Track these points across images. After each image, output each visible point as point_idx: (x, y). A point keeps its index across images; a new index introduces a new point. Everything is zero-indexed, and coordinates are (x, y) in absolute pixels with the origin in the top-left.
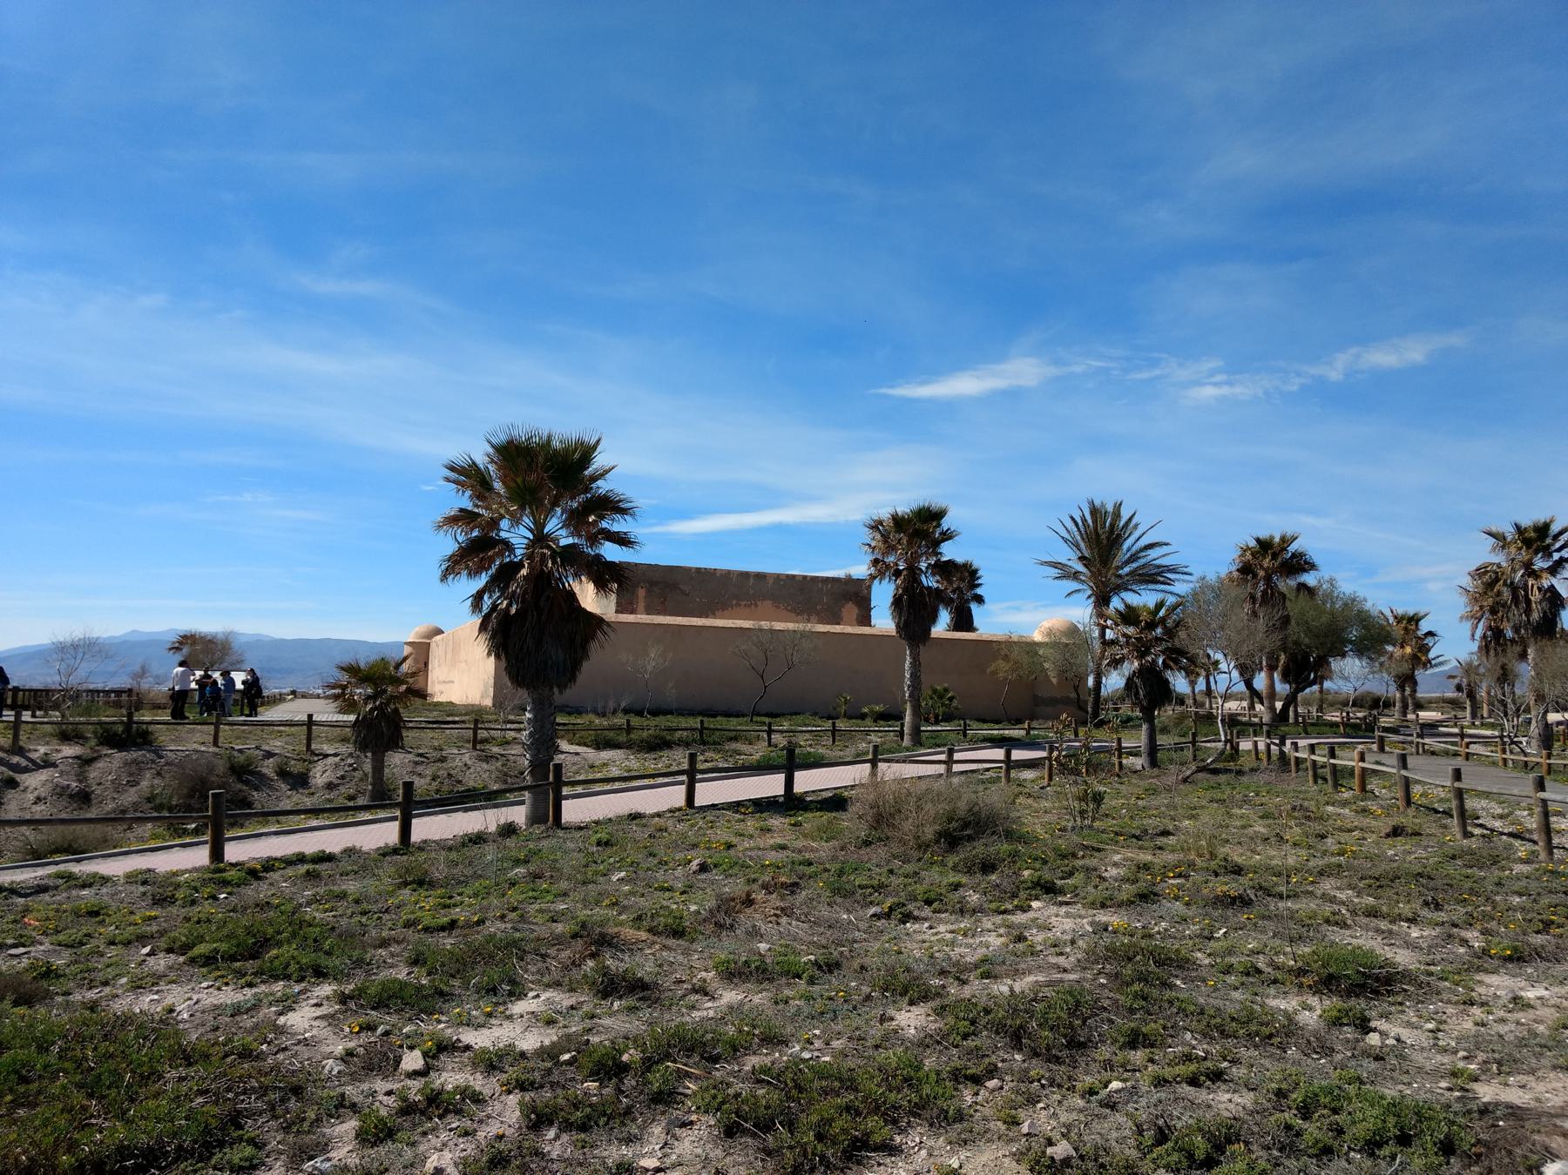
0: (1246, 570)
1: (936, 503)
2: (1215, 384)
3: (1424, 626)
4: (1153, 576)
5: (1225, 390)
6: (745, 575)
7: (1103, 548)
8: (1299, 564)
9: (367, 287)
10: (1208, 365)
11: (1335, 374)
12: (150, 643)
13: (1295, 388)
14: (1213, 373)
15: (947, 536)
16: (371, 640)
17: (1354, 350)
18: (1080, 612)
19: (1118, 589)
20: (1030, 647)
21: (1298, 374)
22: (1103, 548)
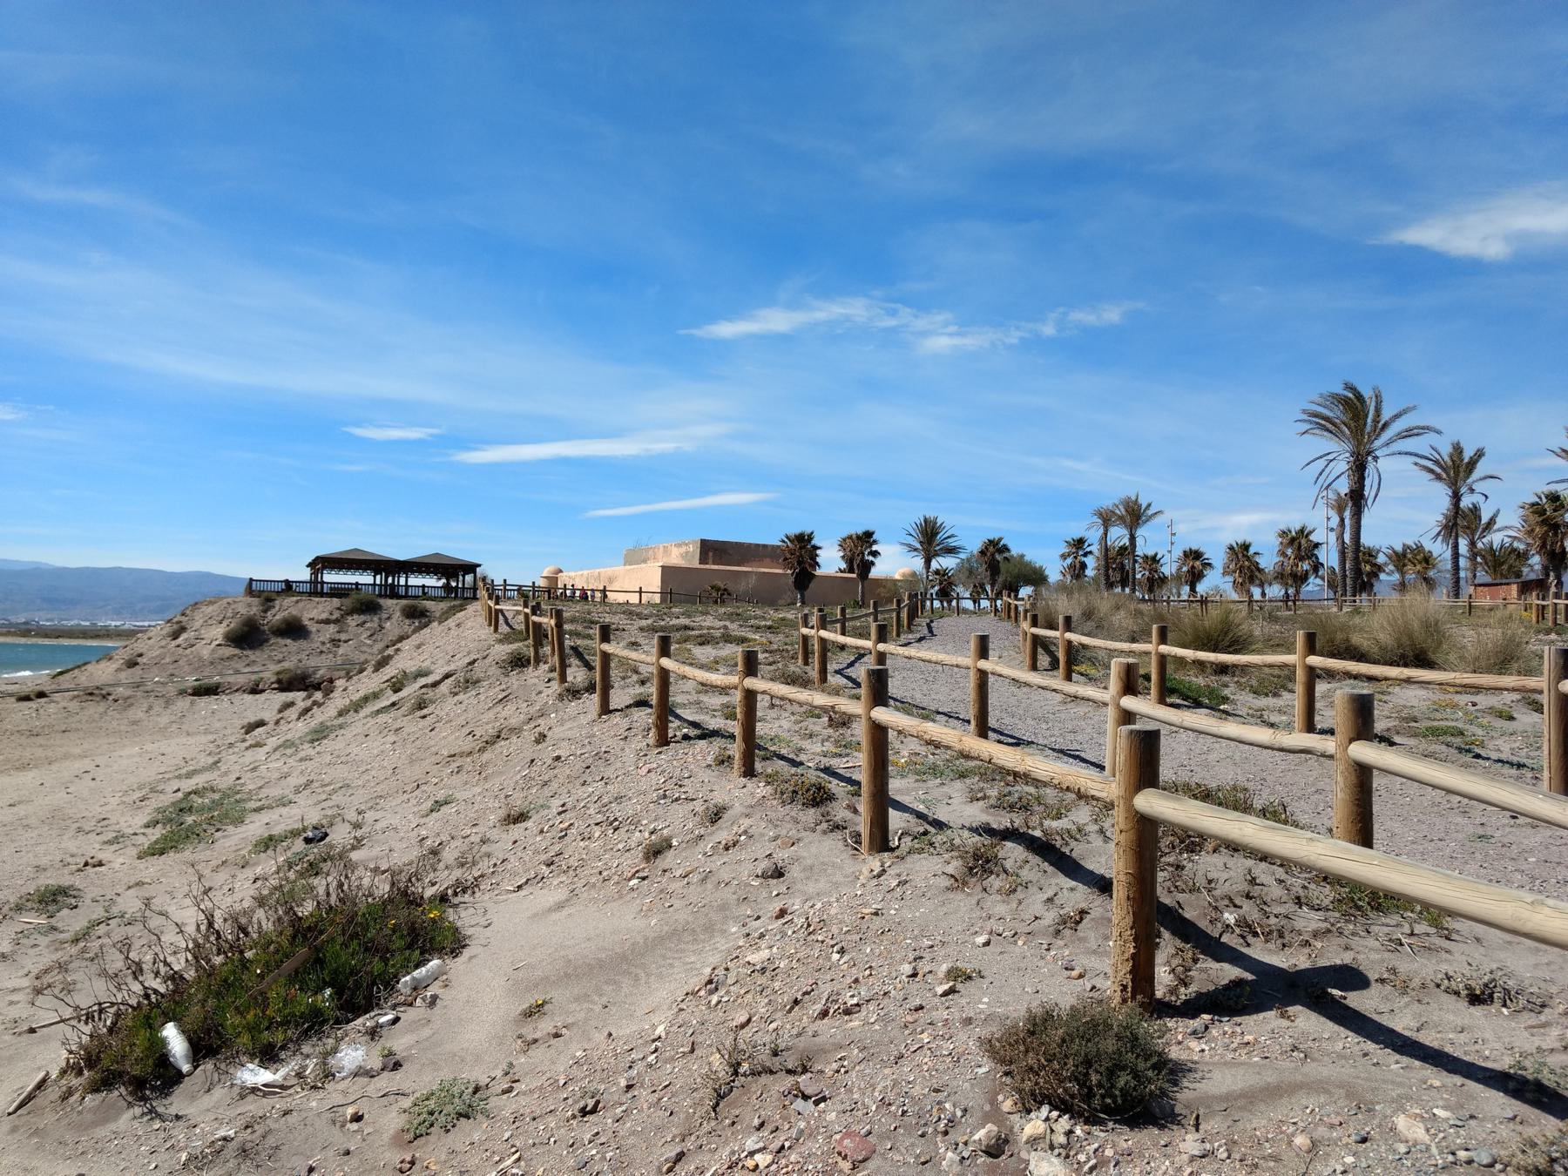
0: (982, 553)
1: (871, 529)
2: (950, 335)
3: (1252, 551)
4: (951, 551)
5: (957, 341)
6: (758, 546)
7: (930, 538)
8: (1006, 549)
9: (94, 197)
10: (940, 318)
11: (1049, 330)
12: (234, 580)
13: (1015, 341)
14: (946, 325)
15: (875, 542)
16: (125, 565)
17: (1061, 310)
18: (918, 563)
19: (937, 555)
20: (895, 581)
21: (1017, 328)
22: (930, 538)
